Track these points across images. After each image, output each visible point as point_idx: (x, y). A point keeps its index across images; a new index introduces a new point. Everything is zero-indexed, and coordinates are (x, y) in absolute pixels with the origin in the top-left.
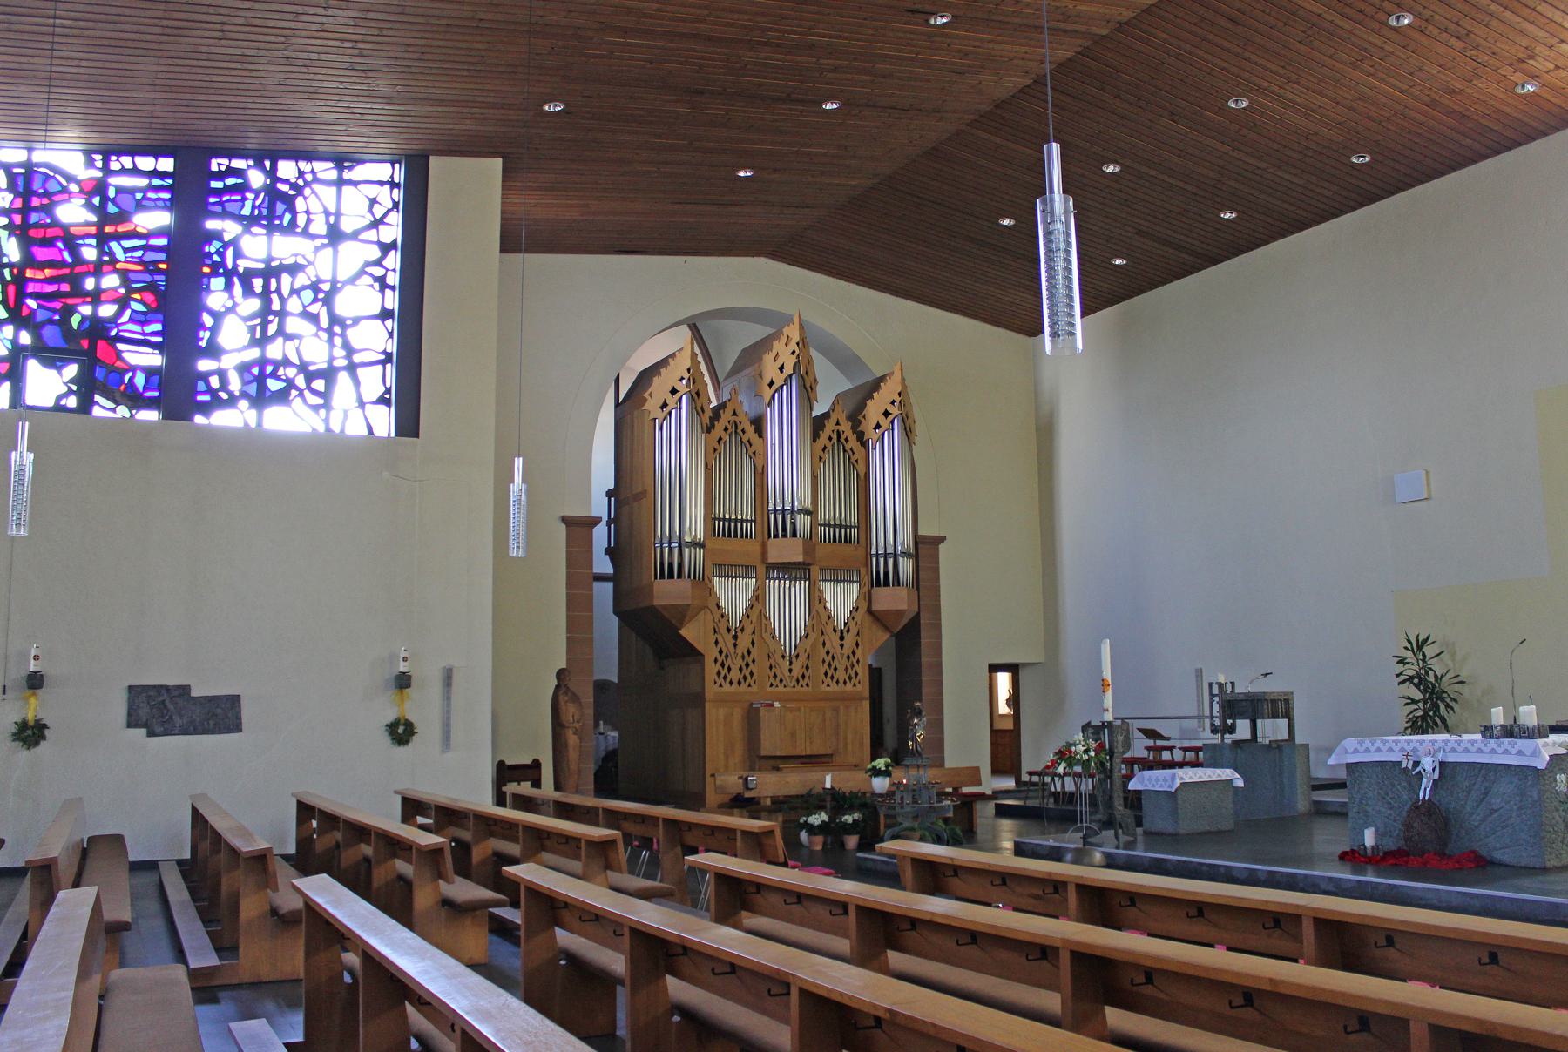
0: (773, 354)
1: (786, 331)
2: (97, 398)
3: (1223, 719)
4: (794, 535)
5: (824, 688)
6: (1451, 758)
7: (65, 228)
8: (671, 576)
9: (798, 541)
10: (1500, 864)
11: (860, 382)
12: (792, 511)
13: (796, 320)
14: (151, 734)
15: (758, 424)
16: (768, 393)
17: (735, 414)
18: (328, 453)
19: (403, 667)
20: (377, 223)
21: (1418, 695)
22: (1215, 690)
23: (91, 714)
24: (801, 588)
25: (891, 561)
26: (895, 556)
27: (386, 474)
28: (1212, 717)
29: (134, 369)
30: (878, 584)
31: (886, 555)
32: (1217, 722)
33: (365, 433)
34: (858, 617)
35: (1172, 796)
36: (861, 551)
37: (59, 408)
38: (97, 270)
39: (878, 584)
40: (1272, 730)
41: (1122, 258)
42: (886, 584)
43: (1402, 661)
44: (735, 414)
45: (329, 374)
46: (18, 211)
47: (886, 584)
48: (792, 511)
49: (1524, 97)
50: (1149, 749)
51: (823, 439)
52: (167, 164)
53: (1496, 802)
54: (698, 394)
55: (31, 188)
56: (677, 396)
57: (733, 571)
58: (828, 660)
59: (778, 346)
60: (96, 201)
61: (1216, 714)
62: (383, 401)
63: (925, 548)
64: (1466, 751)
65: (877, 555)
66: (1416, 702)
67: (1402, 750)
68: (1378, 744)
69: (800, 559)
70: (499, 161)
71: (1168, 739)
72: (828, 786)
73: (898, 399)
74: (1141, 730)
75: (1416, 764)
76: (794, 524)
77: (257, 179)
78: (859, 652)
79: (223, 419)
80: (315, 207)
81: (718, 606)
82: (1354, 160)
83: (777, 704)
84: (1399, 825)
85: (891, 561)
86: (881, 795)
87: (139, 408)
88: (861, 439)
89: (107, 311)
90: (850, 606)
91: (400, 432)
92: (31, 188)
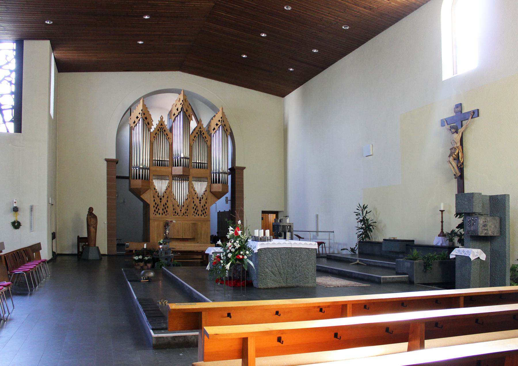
8: (136, 179)
9: (182, 167)
15: (171, 130)
17: (200, 128)
19: (15, 205)
20: (8, 63)
24: (185, 184)
25: (218, 175)
27: (10, 145)
30: (214, 183)
33: (6, 131)
36: (208, 171)
39: (214, 183)
47: (216, 183)
54: (146, 118)
57: (161, 177)
58: (195, 208)
62: (11, 121)
63: (235, 172)
70: (49, 41)
72: (145, 247)
73: (221, 120)
78: (206, 205)
81: (155, 189)
85: (218, 175)
90: (204, 190)
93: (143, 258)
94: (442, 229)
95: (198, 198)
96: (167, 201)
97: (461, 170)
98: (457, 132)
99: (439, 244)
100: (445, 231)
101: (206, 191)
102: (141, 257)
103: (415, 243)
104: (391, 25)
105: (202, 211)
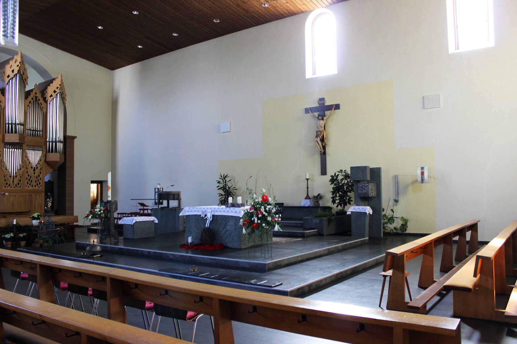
0: (10, 65)
1: (15, 57)
3: (159, 200)
4: (16, 132)
5: (27, 188)
6: (216, 214)
9: (17, 135)
10: (231, 248)
11: (48, 79)
12: (15, 124)
13: (20, 54)
16: (7, 80)
21: (223, 193)
22: (157, 191)
25: (54, 144)
26: (56, 142)
28: (155, 199)
31: (52, 142)
32: (157, 201)
34: (41, 163)
35: (132, 226)
36: (43, 140)
40: (173, 204)
41: (141, 45)
42: (52, 152)
43: (219, 182)
44: (36, 94)
48: (15, 124)
49: (265, 8)
50: (140, 210)
51: (30, 98)
53: (228, 228)
56: (56, 93)
59: (12, 63)
61: (156, 198)
63: (68, 141)
64: (220, 211)
65: (49, 141)
66: (222, 195)
67: (202, 211)
68: (195, 209)
69: (18, 141)
71: (148, 206)
73: (59, 87)
74: (139, 203)
75: (206, 215)
76: (16, 128)
78: (41, 176)
82: (215, 21)
83: (7, 194)
84: (200, 236)
85: (54, 144)
86: (35, 226)
93: (15, 235)
94: (308, 194)
95: (32, 168)
96: (40, 173)
97: (324, 147)
98: (323, 119)
99: (307, 205)
100: (311, 195)
101: (40, 160)
102: (12, 235)
103: (285, 205)
104: (254, 26)
105: (36, 182)
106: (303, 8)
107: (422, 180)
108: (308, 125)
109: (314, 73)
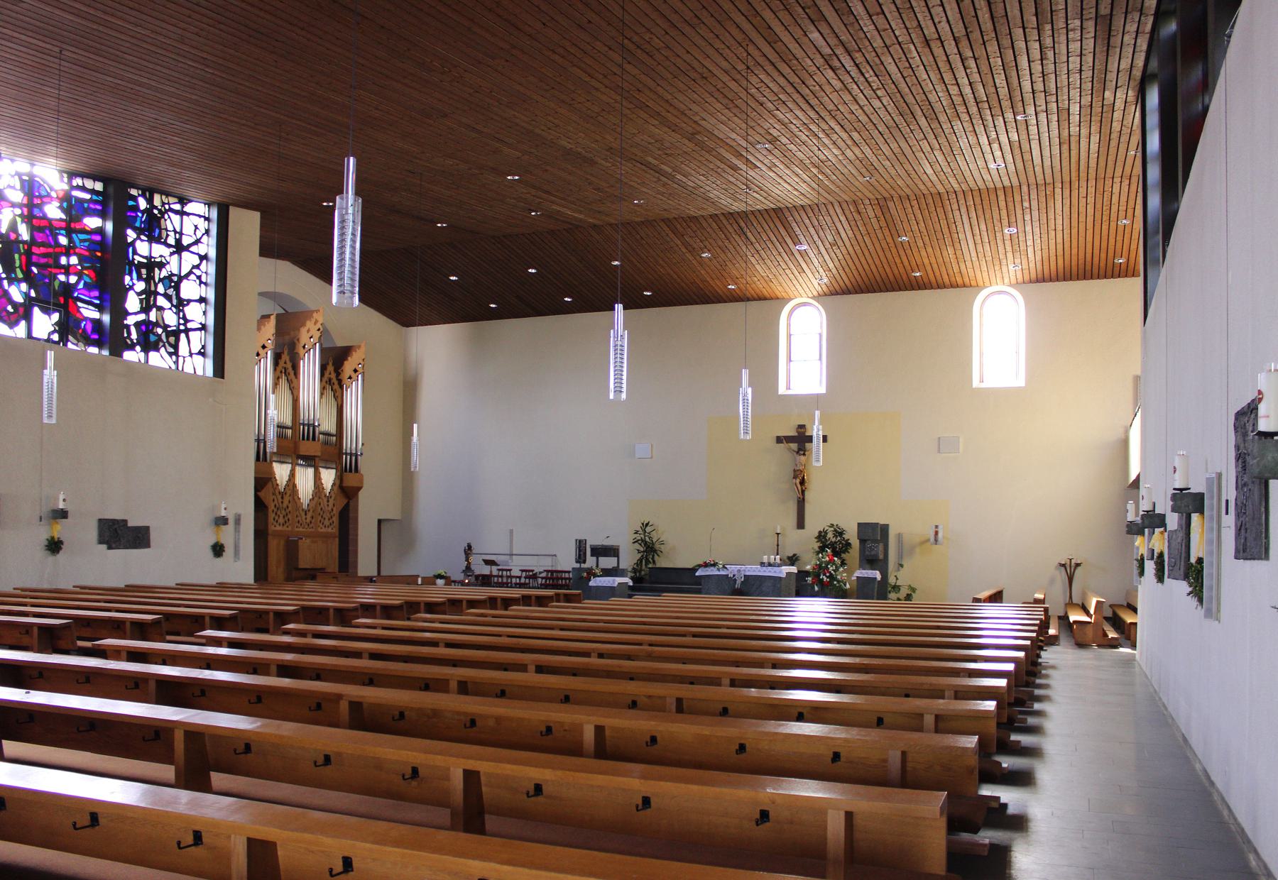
2: (70, 338)
4: (314, 439)
7: (49, 221)
14: (110, 548)
18: (176, 378)
23: (80, 533)
29: (86, 319)
37: (49, 340)
38: (68, 251)
45: (176, 334)
46: (25, 205)
52: (99, 186)
55: (31, 188)
60: (65, 205)
63: (1200, 561)
77: (143, 204)
79: (129, 356)
80: (170, 227)
87: (89, 345)
88: (340, 382)
89: (73, 279)
91: (215, 375)
92: (31, 188)
106: (779, 291)
107: (936, 540)
108: (778, 460)
109: (788, 388)
